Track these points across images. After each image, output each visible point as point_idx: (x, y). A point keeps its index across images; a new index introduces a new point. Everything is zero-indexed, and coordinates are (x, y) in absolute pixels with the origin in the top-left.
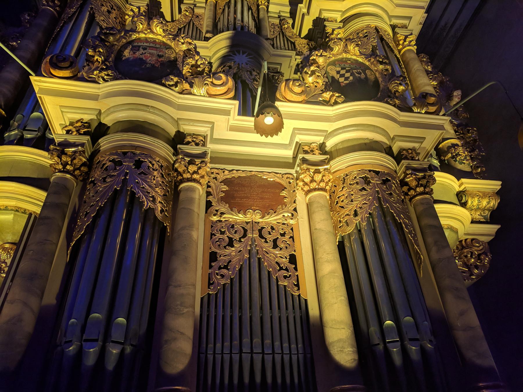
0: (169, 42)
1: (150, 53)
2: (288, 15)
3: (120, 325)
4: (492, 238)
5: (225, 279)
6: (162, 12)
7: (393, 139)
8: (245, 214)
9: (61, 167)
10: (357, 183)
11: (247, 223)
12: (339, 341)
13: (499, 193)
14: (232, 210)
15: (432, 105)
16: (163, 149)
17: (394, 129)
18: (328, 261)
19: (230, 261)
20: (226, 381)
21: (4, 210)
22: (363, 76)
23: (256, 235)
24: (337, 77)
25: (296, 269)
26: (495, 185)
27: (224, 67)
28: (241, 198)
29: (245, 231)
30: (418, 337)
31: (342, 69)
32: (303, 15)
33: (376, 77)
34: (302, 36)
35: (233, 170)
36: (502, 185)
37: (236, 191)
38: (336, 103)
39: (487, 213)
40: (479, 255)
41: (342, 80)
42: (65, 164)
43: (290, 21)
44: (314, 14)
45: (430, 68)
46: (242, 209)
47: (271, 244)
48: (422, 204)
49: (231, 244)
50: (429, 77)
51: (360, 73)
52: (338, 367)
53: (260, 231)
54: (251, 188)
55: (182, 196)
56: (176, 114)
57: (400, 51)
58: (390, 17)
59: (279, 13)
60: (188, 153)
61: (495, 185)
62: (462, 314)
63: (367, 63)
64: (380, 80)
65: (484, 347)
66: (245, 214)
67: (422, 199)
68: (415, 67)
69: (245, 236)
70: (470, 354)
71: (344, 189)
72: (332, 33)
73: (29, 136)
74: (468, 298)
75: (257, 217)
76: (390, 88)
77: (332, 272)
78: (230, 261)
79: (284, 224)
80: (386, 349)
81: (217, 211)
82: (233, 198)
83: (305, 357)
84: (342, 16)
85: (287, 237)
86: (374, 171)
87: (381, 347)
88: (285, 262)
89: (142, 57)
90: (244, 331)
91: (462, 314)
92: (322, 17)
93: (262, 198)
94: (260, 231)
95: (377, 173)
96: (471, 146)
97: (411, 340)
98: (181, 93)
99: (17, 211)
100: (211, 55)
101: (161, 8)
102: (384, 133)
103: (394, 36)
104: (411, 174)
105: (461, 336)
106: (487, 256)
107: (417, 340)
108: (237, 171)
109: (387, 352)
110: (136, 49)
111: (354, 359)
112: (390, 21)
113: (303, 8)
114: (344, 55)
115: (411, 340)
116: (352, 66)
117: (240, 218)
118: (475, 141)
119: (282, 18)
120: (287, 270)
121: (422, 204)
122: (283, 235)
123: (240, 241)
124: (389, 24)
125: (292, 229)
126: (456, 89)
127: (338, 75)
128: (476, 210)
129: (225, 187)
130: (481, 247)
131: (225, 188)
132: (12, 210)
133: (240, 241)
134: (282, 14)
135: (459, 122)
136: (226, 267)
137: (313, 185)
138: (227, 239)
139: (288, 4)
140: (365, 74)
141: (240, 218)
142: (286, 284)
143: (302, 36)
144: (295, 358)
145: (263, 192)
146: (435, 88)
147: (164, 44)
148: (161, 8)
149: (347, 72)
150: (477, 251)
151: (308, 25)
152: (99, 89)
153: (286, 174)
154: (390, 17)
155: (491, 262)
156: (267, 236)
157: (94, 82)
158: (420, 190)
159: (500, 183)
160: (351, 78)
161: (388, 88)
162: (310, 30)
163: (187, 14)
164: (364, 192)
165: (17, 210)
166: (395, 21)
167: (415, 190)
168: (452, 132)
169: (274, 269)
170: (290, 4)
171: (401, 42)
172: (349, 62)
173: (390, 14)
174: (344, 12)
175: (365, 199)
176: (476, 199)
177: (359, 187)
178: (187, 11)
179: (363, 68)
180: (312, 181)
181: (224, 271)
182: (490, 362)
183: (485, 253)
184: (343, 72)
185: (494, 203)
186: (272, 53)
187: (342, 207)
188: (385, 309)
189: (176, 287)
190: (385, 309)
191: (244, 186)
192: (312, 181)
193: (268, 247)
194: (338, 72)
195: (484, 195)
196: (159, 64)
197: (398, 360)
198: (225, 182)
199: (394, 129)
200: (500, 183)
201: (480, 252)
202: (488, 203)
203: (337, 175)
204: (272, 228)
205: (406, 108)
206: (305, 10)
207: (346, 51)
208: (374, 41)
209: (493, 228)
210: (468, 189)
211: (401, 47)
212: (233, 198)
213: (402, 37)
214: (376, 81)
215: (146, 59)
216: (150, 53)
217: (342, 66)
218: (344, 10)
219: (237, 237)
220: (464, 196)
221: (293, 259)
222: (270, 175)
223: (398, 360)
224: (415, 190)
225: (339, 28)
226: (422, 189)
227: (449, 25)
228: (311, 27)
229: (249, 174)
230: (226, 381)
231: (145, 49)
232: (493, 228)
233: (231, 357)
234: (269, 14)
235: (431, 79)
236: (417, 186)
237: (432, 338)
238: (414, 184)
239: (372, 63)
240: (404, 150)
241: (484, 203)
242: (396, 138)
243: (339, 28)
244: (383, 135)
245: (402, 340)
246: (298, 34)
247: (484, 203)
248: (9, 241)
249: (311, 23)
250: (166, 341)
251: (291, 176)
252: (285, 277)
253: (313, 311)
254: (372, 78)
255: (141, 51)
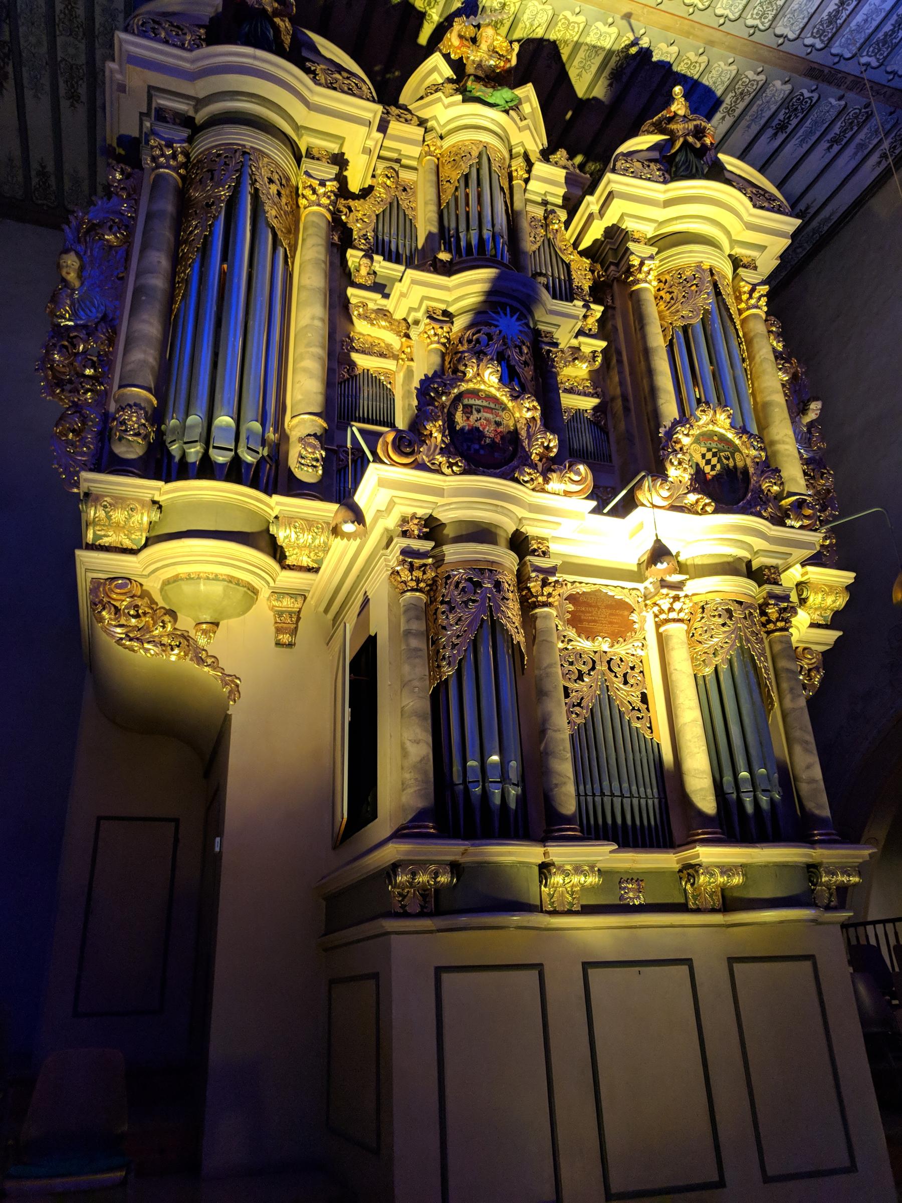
0: (505, 399)
1: (485, 419)
2: (560, 202)
3: (494, 764)
4: (829, 648)
5: (580, 718)
6: (346, 177)
7: (757, 553)
8: (593, 640)
9: (413, 584)
10: (720, 616)
11: (595, 652)
12: (702, 789)
13: (848, 588)
14: (579, 636)
15: (808, 517)
16: (509, 560)
17: (758, 543)
18: (690, 708)
19: (582, 699)
20: (592, 822)
21: (213, 579)
22: (731, 463)
23: (605, 668)
24: (702, 463)
25: (648, 709)
26: (847, 577)
27: (478, 332)
28: (589, 621)
29: (594, 662)
30: (769, 788)
31: (709, 450)
32: (591, 217)
33: (746, 465)
34: (581, 248)
35: (574, 582)
36: (855, 578)
37: (582, 612)
38: (704, 512)
39: (829, 614)
40: (810, 670)
41: (707, 469)
42: (418, 581)
43: (563, 215)
44: (611, 218)
45: (780, 347)
46: (591, 635)
47: (621, 679)
48: (781, 642)
49: (580, 677)
50: (778, 364)
51: (727, 459)
52: (700, 813)
53: (609, 662)
54: (599, 608)
55: (539, 624)
56: (521, 512)
57: (740, 312)
58: (733, 243)
59: (545, 194)
60: (537, 566)
61: (847, 577)
62: (808, 767)
63: (737, 442)
64: (751, 470)
65: (824, 799)
66: (593, 640)
67: (782, 636)
68: (761, 353)
69: (593, 668)
70: (810, 805)
71: (703, 621)
72: (640, 270)
73: (221, 458)
74: (815, 752)
75: (605, 647)
76: (764, 487)
77: (694, 721)
78: (582, 699)
79: (633, 655)
80: (739, 797)
81: (564, 637)
82: (581, 621)
83: (660, 802)
84: (656, 230)
85: (637, 670)
86: (738, 602)
87: (734, 796)
88: (638, 703)
89: (478, 424)
90: (602, 770)
91: (808, 767)
92: (624, 227)
93: (611, 623)
94: (609, 662)
95: (740, 603)
96: (822, 499)
97: (763, 790)
98: (533, 490)
99: (230, 582)
100: (450, 299)
101: (346, 169)
102: (749, 547)
103: (733, 279)
104: (774, 605)
105: (804, 788)
106: (818, 672)
107: (768, 791)
108: (580, 583)
109: (740, 802)
110: (468, 410)
111: (416, 779)
112: (732, 248)
113: (593, 204)
114: (711, 427)
115: (763, 790)
116: (719, 446)
117: (584, 644)
118: (828, 491)
119: (550, 207)
120: (639, 710)
121: (781, 642)
122: (633, 668)
123: (589, 674)
124: (727, 252)
125: (641, 662)
126: (816, 399)
127: (704, 461)
128: (816, 609)
129: (571, 606)
130: (813, 661)
131: (571, 607)
132: (224, 580)
133: (589, 674)
134: (550, 199)
135: (811, 455)
136: (579, 705)
137: (673, 615)
138: (576, 672)
139: (563, 180)
140: (734, 460)
141: (584, 644)
142: (639, 726)
143: (581, 248)
144: (650, 802)
145: (611, 614)
146: (783, 385)
147: (495, 400)
148: (346, 169)
149: (714, 455)
150: (808, 664)
151: (596, 232)
152: (445, 481)
153: (633, 589)
154: (733, 243)
155: (822, 681)
156: (616, 669)
157: (439, 472)
158: (780, 624)
159: (853, 575)
160: (718, 467)
161: (760, 486)
162: (596, 241)
163: (388, 182)
164: (726, 629)
165: (231, 580)
166: (738, 251)
167: (775, 623)
168: (802, 482)
169: (627, 708)
170: (566, 183)
171: (745, 297)
172: (716, 438)
173: (734, 237)
174: (661, 224)
175: (727, 637)
176: (820, 596)
177: (721, 621)
178: (389, 178)
179: (731, 449)
180: (671, 609)
181: (577, 710)
182: (826, 812)
183: (817, 669)
184: (709, 456)
185: (840, 602)
186: (549, 307)
187: (700, 642)
188: (741, 761)
189: (555, 731)
190: (741, 761)
191: (591, 606)
192: (671, 609)
193: (618, 683)
194: (703, 456)
195: (832, 589)
196: (499, 437)
197: (750, 808)
198: (571, 598)
199: (758, 543)
200: (853, 575)
201: (811, 667)
202: (834, 602)
203: (696, 599)
204: (621, 660)
205: (779, 521)
206: (595, 208)
207: (713, 422)
208: (706, 300)
209: (832, 636)
210: (812, 580)
211: (743, 305)
212: (581, 621)
213: (747, 288)
214: (745, 470)
215: (484, 429)
216: (485, 419)
217: (708, 445)
218: (660, 220)
219: (585, 669)
220: (805, 590)
221: (644, 699)
222: (616, 589)
223: (750, 808)
224: (775, 625)
225: (651, 257)
226: (783, 624)
227: (812, 211)
228: (599, 237)
229: (594, 588)
230: (592, 822)
231: (479, 411)
232: (832, 636)
233: (612, 800)
234: (528, 196)
235: (780, 369)
236: (778, 620)
237: (780, 789)
238: (774, 617)
239: (744, 443)
240: (767, 567)
241: (829, 600)
242: (761, 553)
243: (651, 257)
244: (743, 549)
245: (754, 791)
246: (572, 241)
247: (829, 600)
248: (208, 620)
249: (602, 231)
250: (556, 785)
251: (638, 593)
252: (638, 718)
253: (667, 756)
254: (740, 464)
255: (475, 415)
